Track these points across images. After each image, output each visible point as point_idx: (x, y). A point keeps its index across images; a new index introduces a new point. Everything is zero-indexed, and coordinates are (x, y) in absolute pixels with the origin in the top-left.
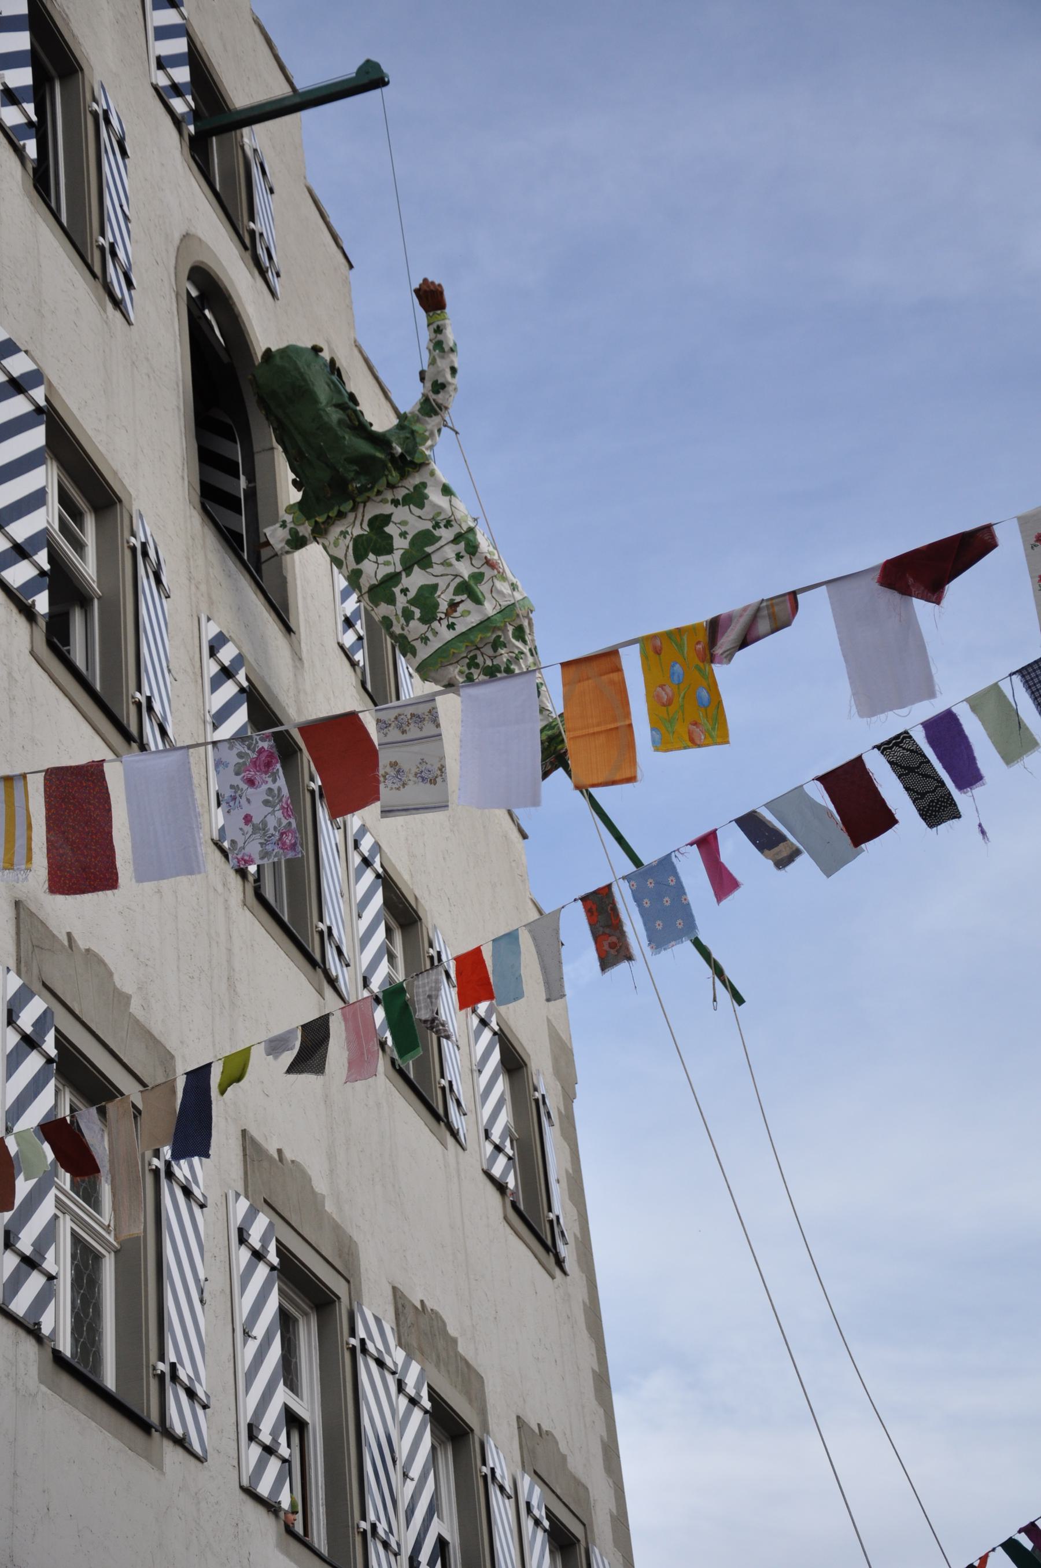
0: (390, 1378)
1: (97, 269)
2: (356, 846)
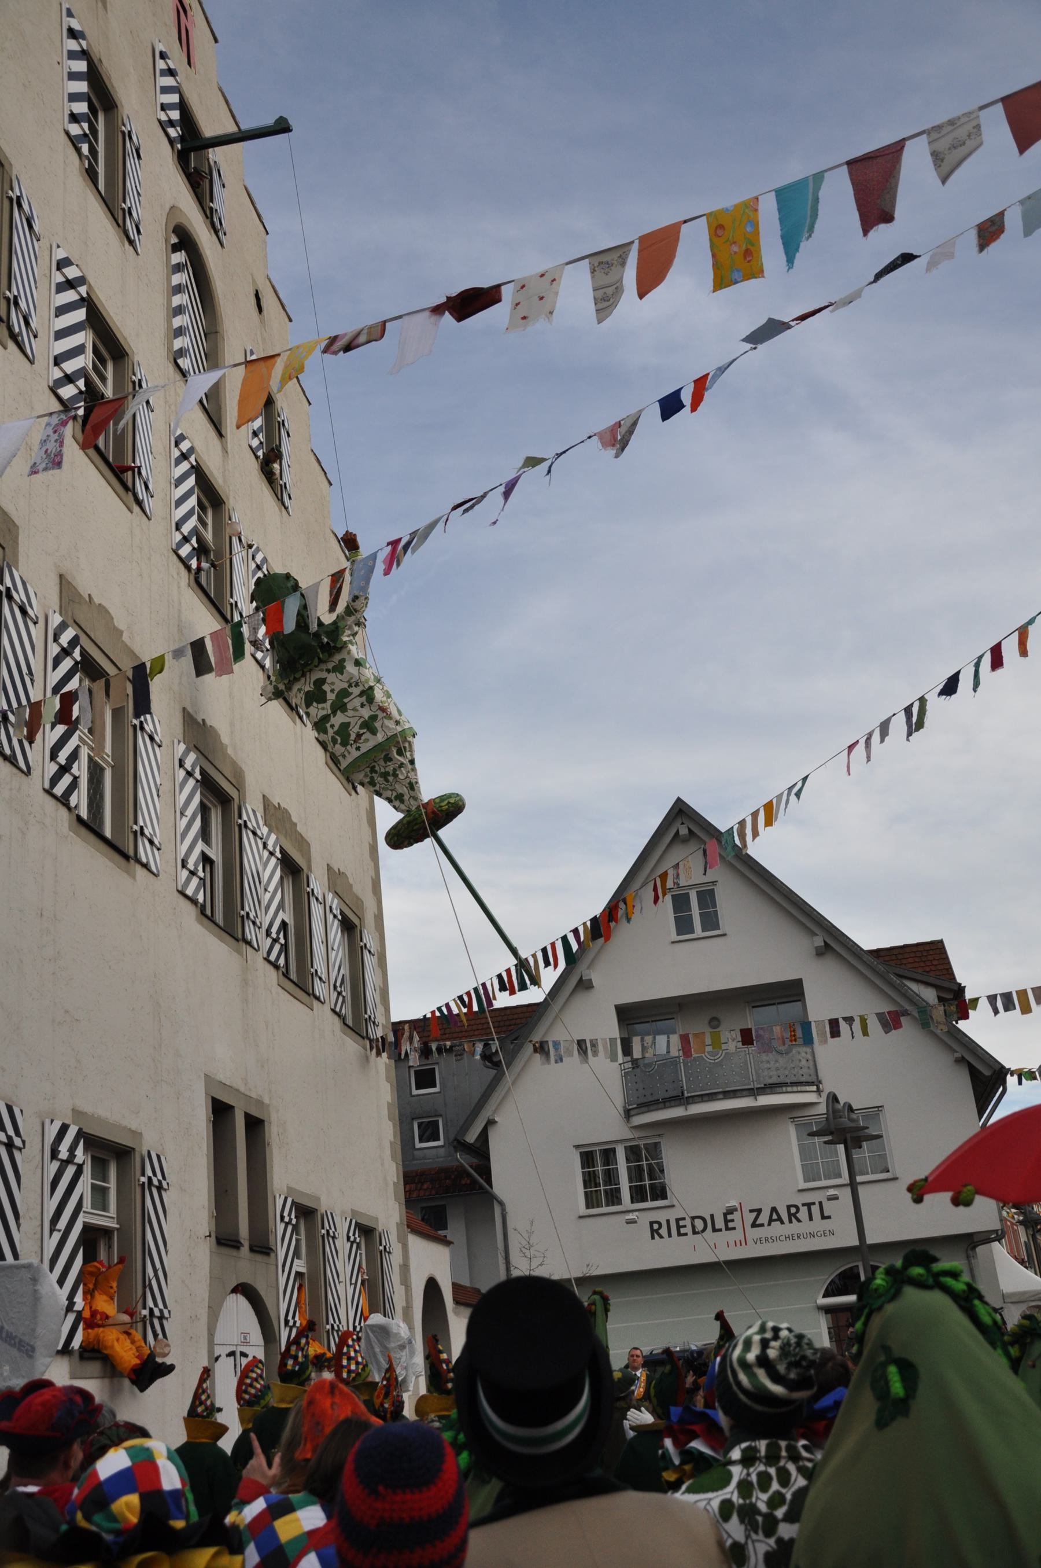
0: (259, 841)
1: (120, 222)
2: (253, 558)
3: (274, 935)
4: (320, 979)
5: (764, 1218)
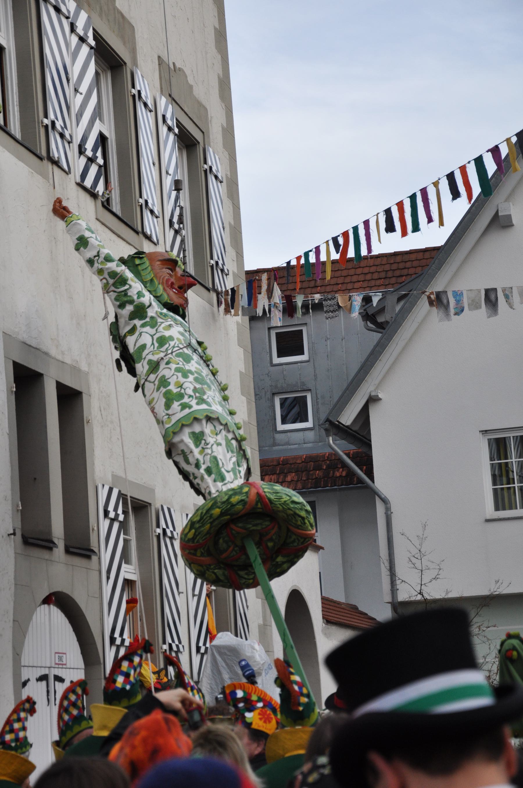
0: (64, 21)
3: (89, 153)
4: (152, 212)
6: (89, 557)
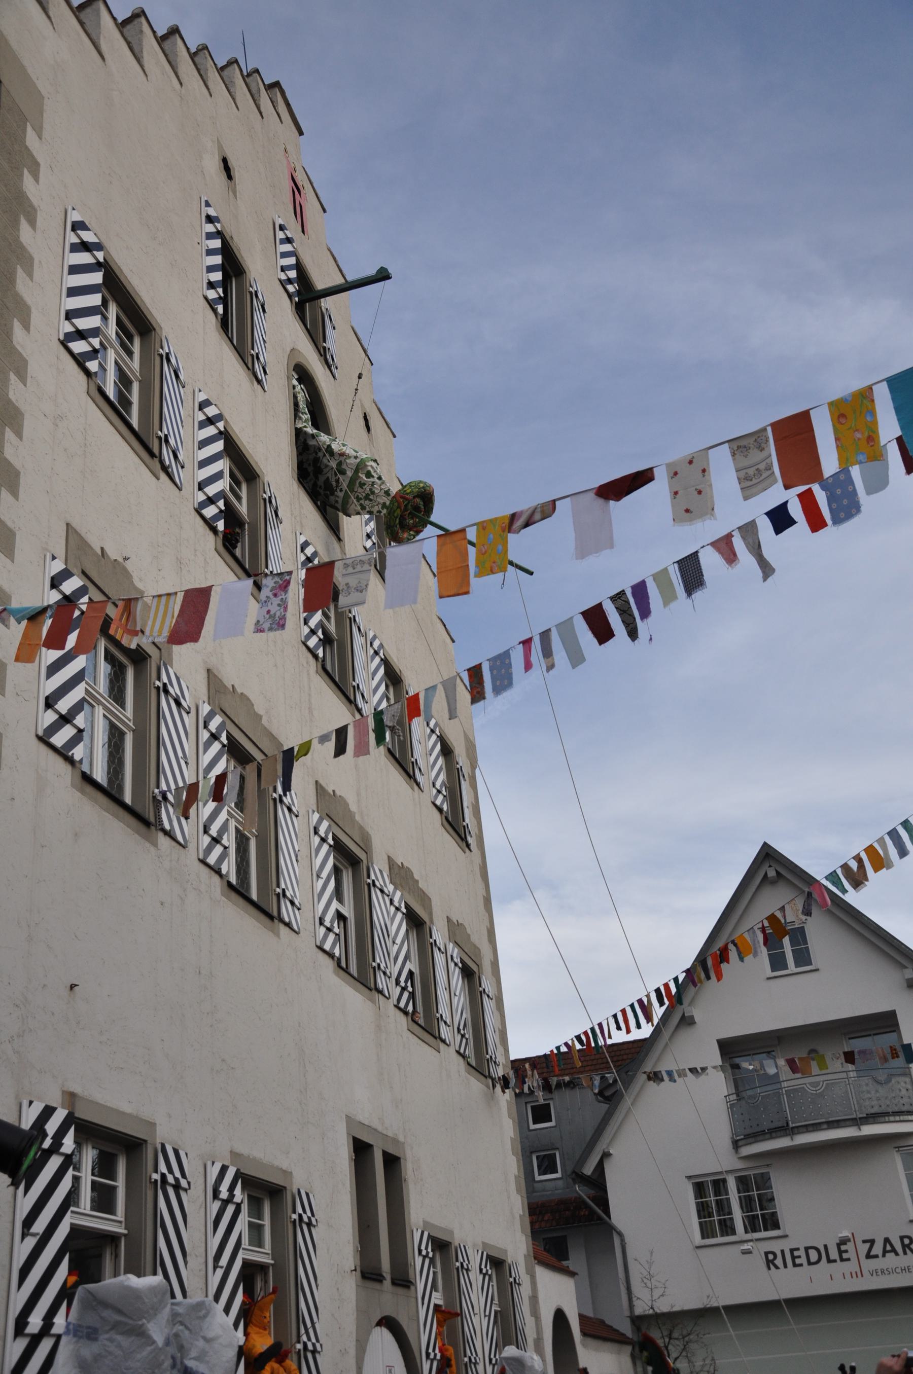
0: (386, 898)
1: (250, 365)
2: (371, 645)
3: (403, 984)
4: (445, 1023)
5: (878, 1249)
6: (408, 1287)
